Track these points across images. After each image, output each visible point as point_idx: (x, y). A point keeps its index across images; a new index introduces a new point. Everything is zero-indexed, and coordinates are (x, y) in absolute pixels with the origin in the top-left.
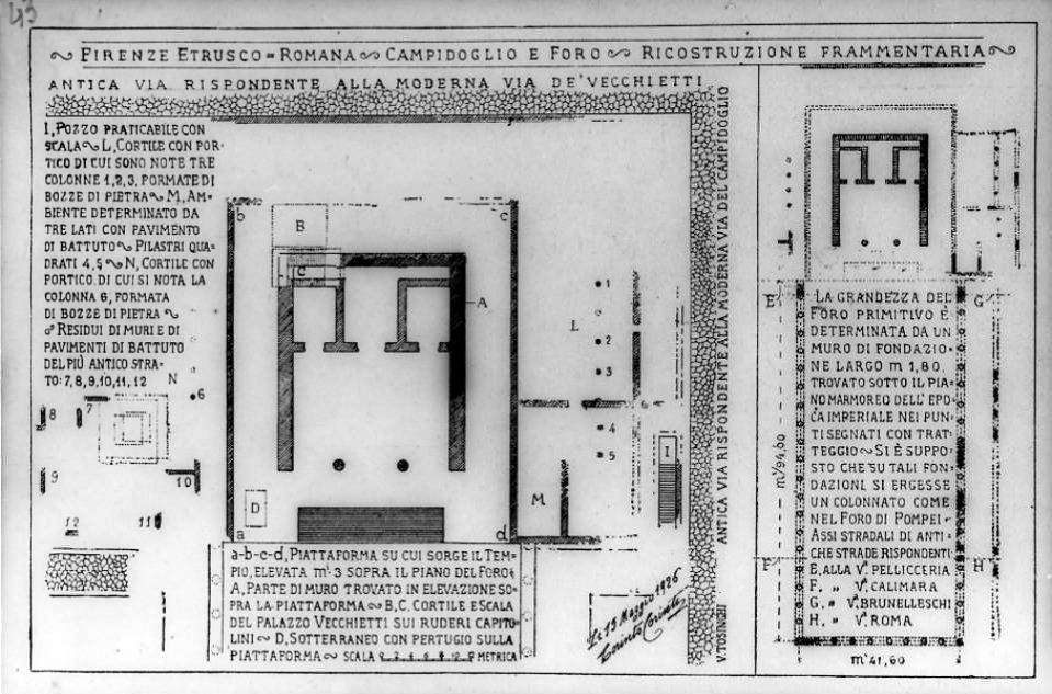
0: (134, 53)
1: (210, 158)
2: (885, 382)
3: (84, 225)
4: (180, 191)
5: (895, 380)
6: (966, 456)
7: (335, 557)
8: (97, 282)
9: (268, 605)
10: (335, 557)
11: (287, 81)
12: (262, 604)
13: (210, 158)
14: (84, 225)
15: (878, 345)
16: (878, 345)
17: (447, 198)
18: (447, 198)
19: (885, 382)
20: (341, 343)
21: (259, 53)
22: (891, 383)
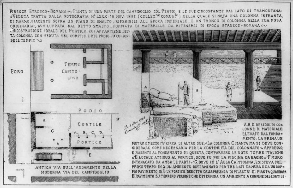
0: (238, 152)
1: (262, 152)
2: (196, 172)
3: (254, 147)
4: (226, 156)
5: (199, 171)
6: (268, 119)
7: (67, 72)
8: (199, 163)
9: (225, 157)
10: (67, 72)
11: (175, 152)
12: (223, 157)
13: (262, 152)
14: (254, 147)
15: (210, 161)
16: (210, 161)
17: (225, 132)
18: (225, 132)
19: (196, 172)
20: (86, 62)
21: (193, 157)
22: (198, 172)
